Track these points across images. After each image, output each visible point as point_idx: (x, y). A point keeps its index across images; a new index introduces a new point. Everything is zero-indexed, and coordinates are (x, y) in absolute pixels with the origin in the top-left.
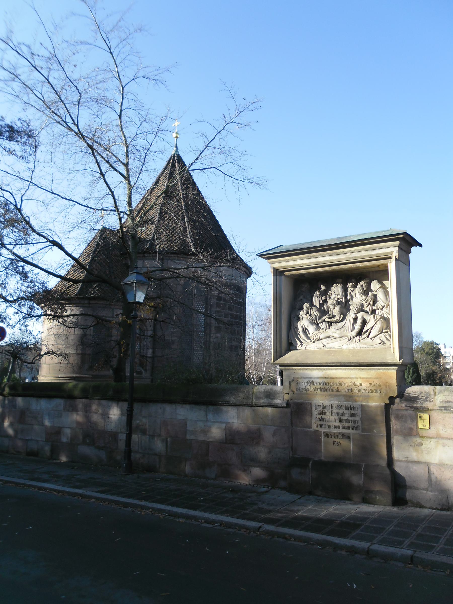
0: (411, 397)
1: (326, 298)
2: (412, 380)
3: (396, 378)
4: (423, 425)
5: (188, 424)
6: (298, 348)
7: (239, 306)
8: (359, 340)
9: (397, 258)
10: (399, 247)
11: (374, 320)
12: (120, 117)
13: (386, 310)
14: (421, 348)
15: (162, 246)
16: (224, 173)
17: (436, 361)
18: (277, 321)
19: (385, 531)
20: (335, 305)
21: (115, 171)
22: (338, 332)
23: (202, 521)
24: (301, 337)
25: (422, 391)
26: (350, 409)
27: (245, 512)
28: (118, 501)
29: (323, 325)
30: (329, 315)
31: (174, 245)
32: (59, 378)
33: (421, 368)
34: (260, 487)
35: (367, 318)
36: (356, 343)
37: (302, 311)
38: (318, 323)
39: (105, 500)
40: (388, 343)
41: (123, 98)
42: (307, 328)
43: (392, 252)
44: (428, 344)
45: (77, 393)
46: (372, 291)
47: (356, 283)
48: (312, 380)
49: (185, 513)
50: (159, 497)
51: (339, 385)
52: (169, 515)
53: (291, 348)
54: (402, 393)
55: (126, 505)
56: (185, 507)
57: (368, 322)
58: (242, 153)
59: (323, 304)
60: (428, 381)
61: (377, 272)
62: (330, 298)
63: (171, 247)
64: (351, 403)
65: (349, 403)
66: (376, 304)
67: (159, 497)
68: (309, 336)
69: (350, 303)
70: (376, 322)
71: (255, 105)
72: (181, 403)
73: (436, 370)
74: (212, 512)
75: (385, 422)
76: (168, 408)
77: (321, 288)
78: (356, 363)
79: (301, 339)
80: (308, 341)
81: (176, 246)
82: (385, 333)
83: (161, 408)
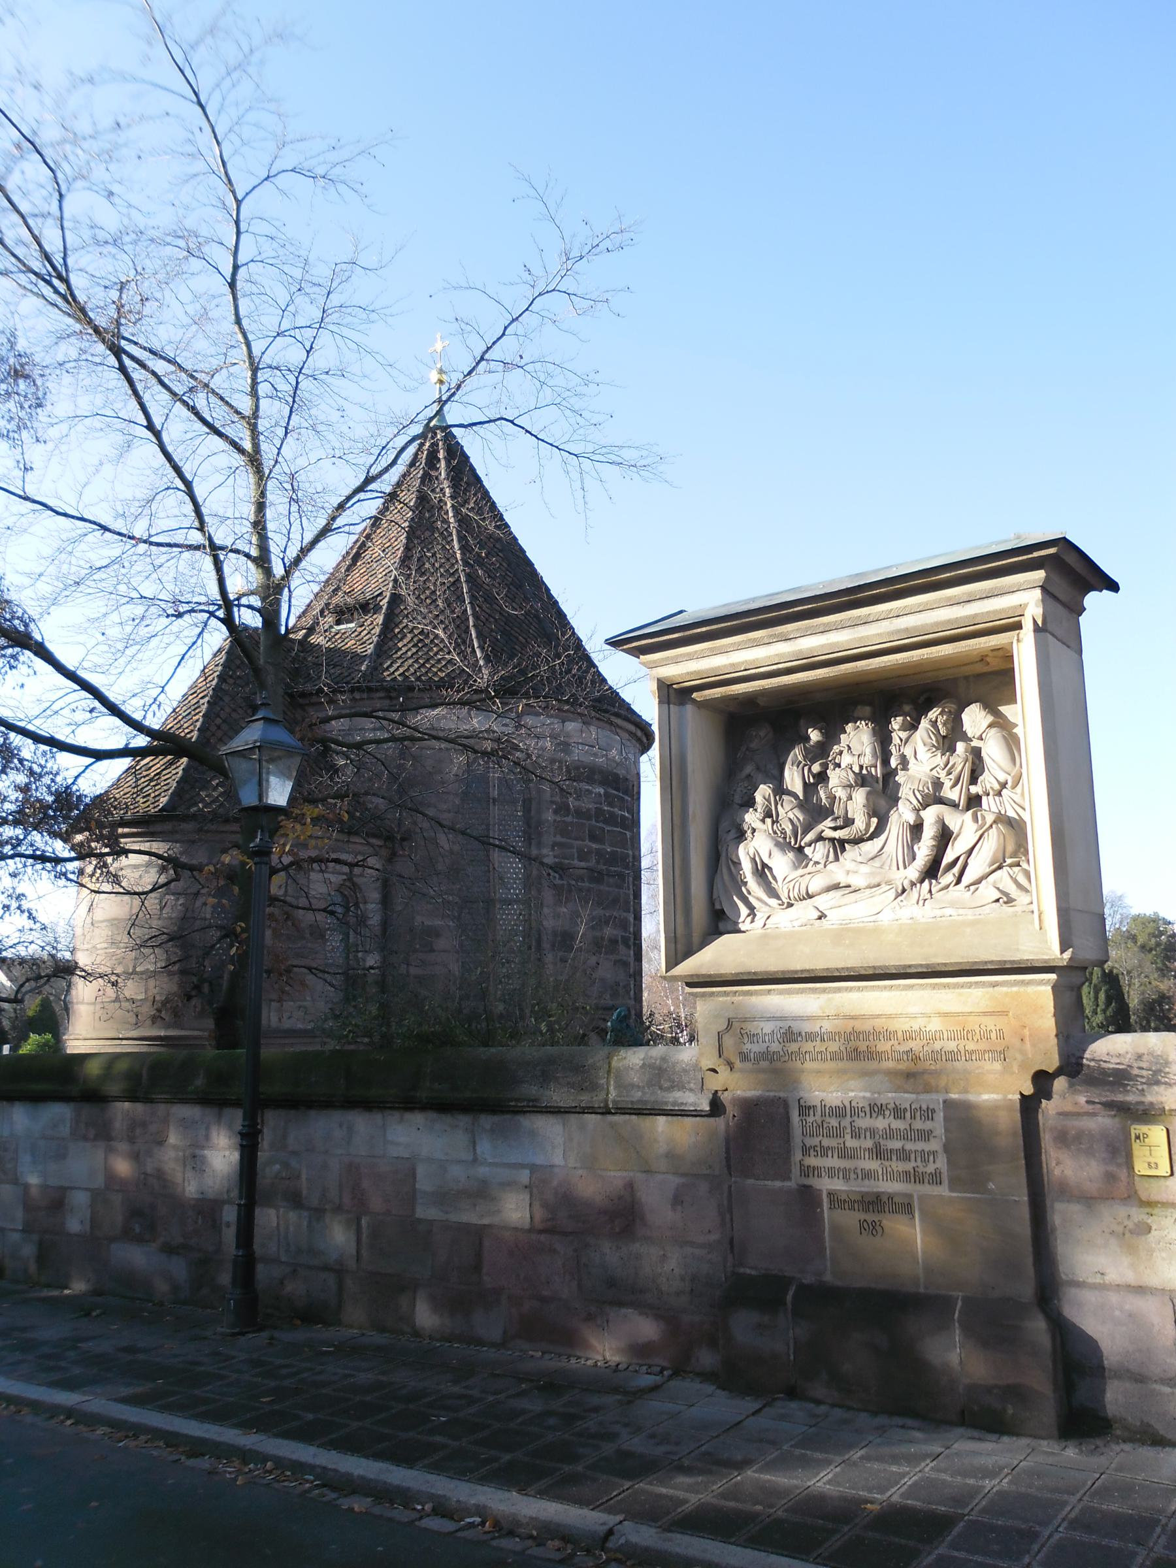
0: (1104, 1072)
1: (825, 767)
2: (1106, 1019)
3: (1052, 1009)
4: (1149, 1164)
5: (421, 1170)
6: (742, 927)
7: (619, 829)
8: (930, 891)
9: (1040, 623)
10: (1043, 588)
11: (975, 826)
12: (232, 285)
13: (1013, 795)
14: (1126, 934)
15: (401, 670)
16: (536, 436)
17: (1167, 967)
18: (675, 842)
19: (1036, 1547)
20: (850, 786)
21: (216, 437)
22: (865, 869)
23: (423, 1509)
24: (749, 893)
25: (1141, 1050)
26: (908, 1115)
27: (567, 1468)
28: (176, 1435)
29: (818, 852)
30: (835, 819)
31: (433, 666)
32: (118, 1042)
33: (1129, 985)
34: (636, 1371)
35: (954, 820)
36: (921, 902)
37: (751, 810)
38: (803, 844)
39: (136, 1430)
40: (1022, 899)
41: (238, 233)
42: (766, 861)
43: (1023, 607)
44: (1143, 924)
45: (114, 1088)
46: (965, 738)
47: (914, 715)
48: (786, 1025)
49: (372, 1477)
50: (310, 1416)
51: (871, 1037)
52: (324, 1486)
53: (721, 926)
54: (1073, 1060)
55: (198, 1447)
56: (378, 1456)
57: (958, 836)
58: (585, 377)
59: (815, 785)
60: (1148, 1022)
61: (980, 676)
62: (839, 765)
63: (427, 672)
64: (913, 1096)
65: (906, 1095)
66: (981, 779)
67: (310, 1416)
68: (776, 887)
69: (900, 778)
70: (980, 832)
71: (618, 239)
72: (398, 1109)
73: (1169, 990)
74: (461, 1474)
75: (1022, 1154)
76: (362, 1123)
77: (808, 739)
78: (921, 965)
79: (751, 899)
80: (773, 902)
81: (440, 670)
82: (1011, 866)
83: (341, 1126)
